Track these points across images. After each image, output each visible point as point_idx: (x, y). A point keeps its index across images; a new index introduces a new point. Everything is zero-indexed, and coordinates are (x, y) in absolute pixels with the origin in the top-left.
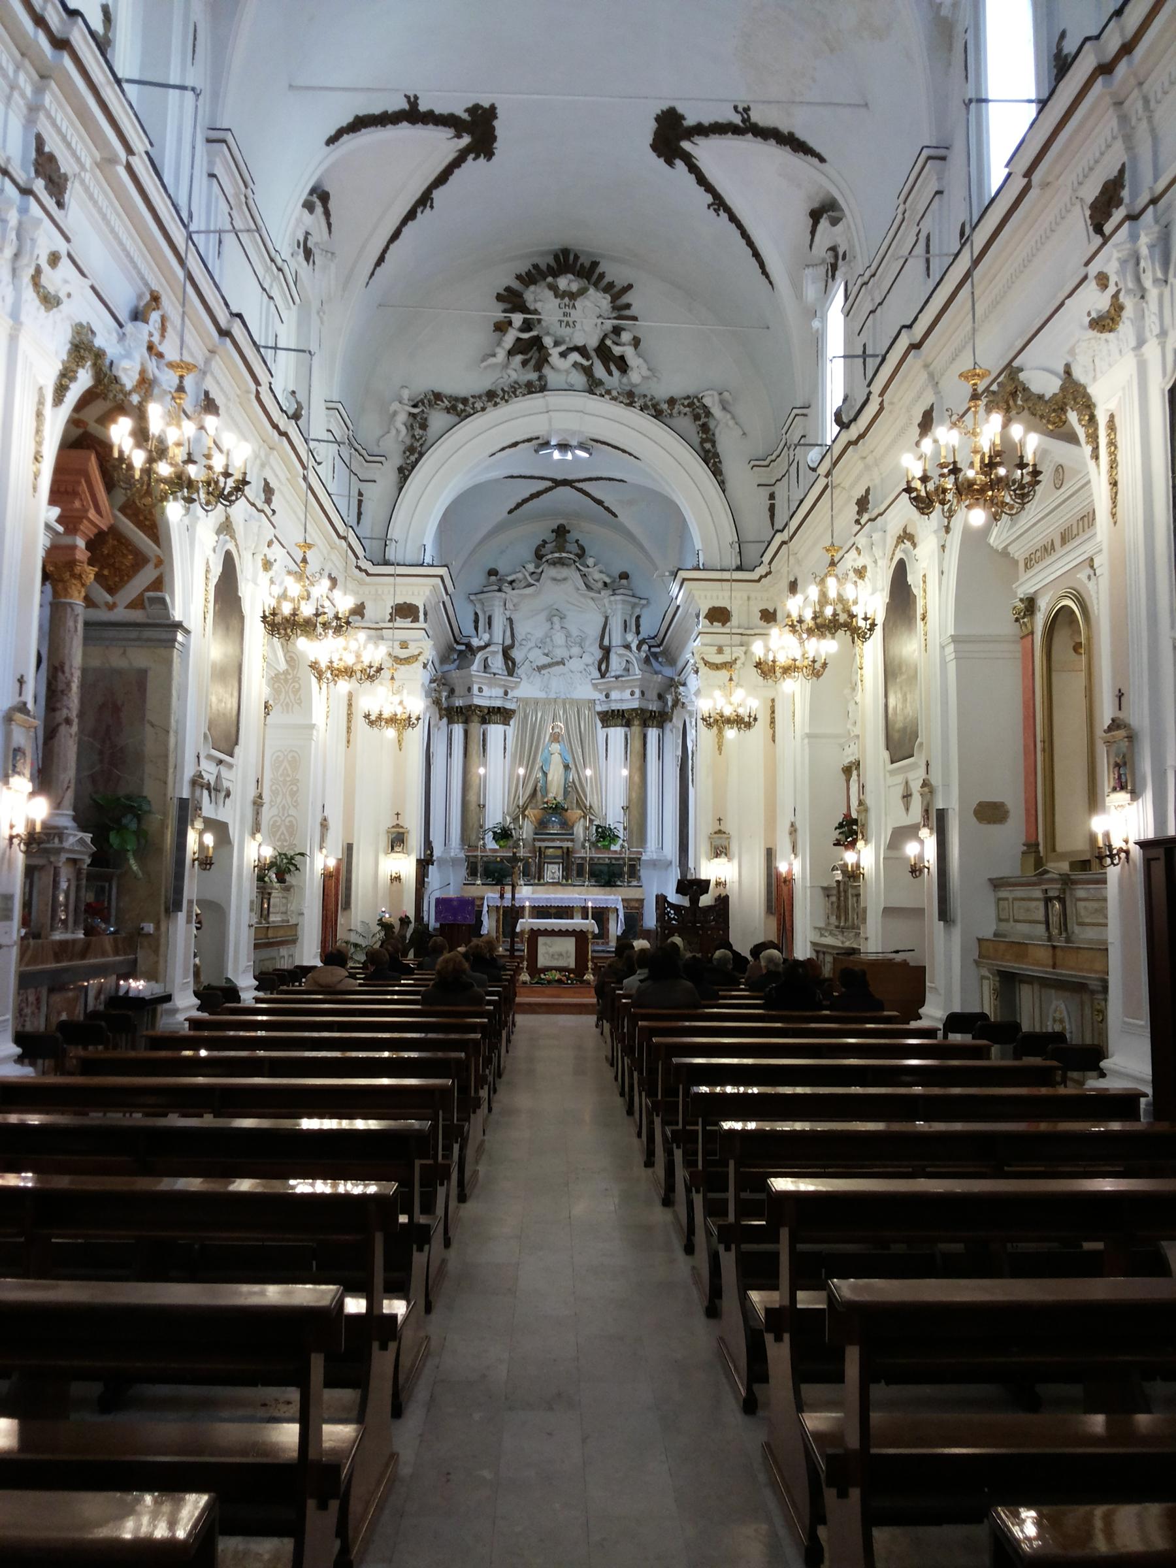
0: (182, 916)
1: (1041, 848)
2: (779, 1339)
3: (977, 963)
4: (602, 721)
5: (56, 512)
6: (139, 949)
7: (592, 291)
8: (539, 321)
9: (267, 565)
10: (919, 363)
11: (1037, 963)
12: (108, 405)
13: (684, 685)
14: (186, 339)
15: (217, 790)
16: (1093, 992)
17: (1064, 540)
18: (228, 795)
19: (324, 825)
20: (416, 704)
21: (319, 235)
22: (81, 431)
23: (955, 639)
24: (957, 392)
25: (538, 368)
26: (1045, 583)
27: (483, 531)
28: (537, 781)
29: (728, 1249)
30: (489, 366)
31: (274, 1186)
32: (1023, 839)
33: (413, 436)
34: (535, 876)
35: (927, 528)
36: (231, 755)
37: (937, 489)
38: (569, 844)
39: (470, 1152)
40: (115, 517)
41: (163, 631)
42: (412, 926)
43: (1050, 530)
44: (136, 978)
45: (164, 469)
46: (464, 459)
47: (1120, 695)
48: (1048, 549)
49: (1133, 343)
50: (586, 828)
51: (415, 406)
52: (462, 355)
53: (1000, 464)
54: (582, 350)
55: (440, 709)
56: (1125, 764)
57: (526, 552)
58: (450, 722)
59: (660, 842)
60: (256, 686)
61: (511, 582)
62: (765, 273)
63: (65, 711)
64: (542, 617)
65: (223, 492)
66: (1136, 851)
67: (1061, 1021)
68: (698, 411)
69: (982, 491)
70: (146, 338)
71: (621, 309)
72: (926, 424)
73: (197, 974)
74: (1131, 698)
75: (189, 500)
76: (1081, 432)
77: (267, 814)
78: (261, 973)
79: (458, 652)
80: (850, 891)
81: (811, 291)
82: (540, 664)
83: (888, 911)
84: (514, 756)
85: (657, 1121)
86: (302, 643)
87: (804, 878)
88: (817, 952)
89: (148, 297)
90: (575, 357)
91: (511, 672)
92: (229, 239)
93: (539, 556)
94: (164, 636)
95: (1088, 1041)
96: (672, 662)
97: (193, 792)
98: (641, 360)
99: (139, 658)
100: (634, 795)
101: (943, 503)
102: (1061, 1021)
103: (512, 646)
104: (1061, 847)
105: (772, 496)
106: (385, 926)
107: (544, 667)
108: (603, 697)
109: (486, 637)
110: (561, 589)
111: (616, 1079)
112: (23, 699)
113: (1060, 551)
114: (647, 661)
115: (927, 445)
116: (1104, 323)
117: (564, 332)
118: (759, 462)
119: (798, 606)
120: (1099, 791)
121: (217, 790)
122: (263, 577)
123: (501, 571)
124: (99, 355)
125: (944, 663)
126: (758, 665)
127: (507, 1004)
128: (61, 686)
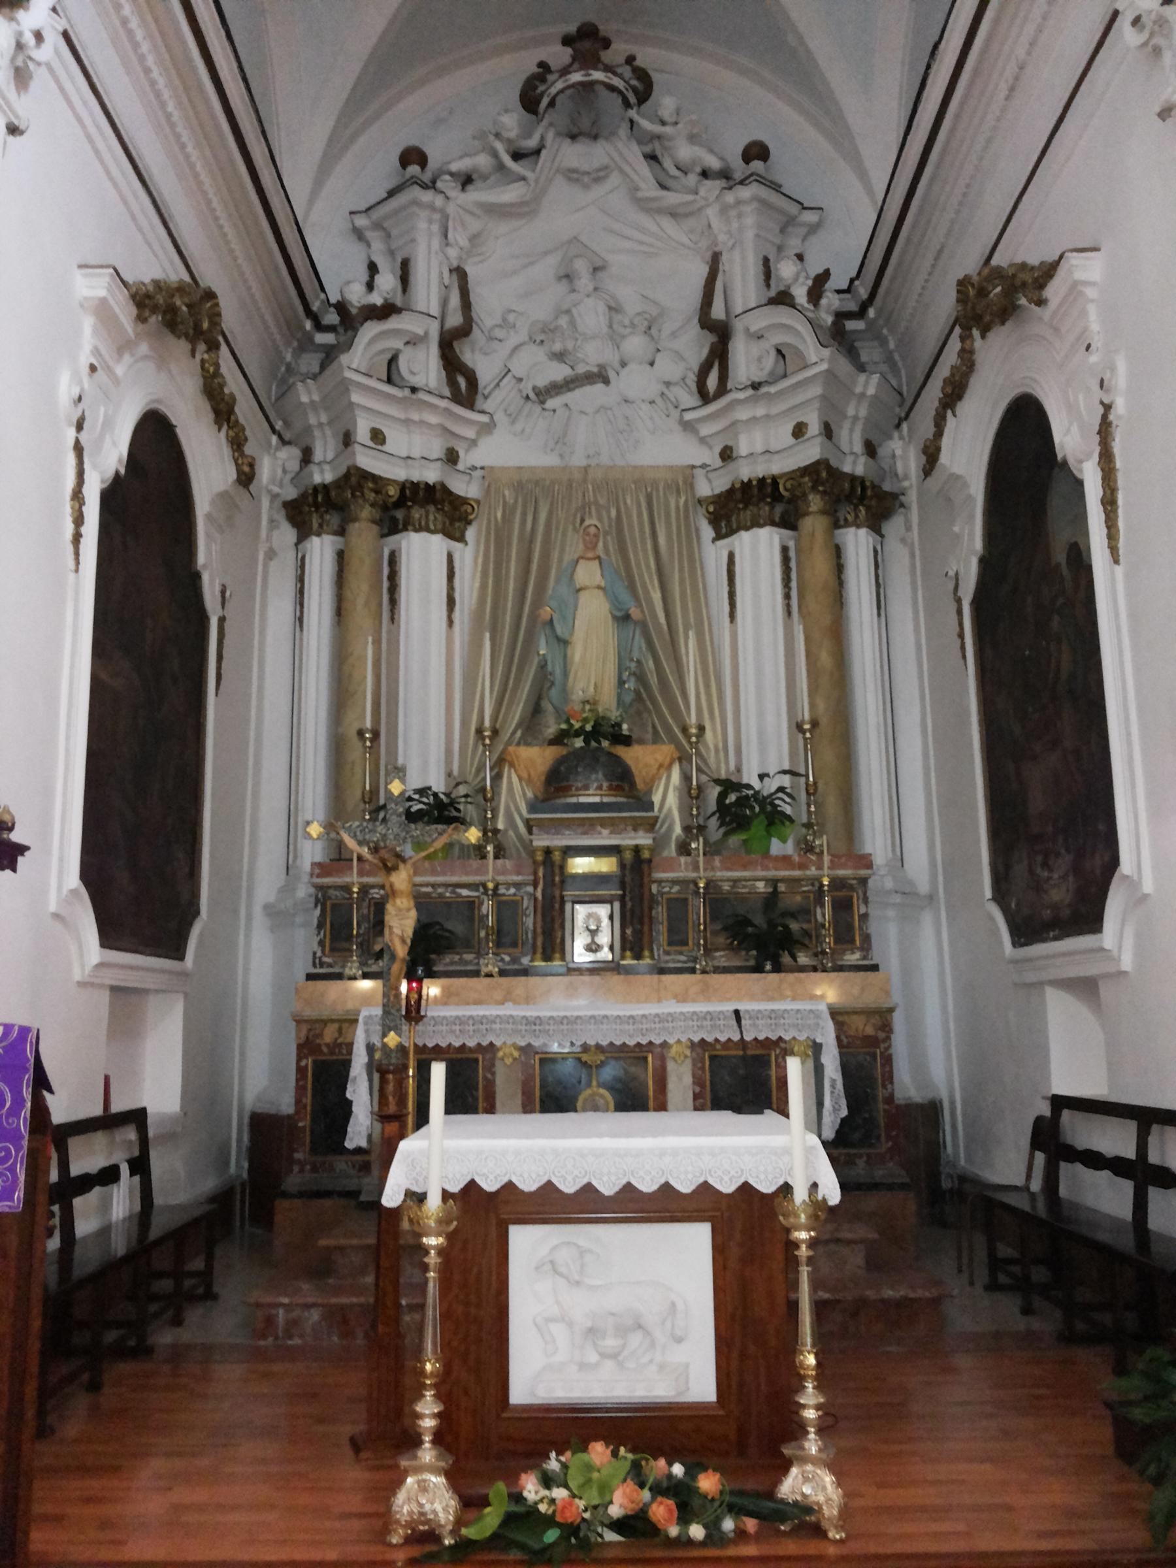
38: (643, 839)
58: (304, 532)
82: (542, 382)
103: (465, 331)
107: (555, 389)
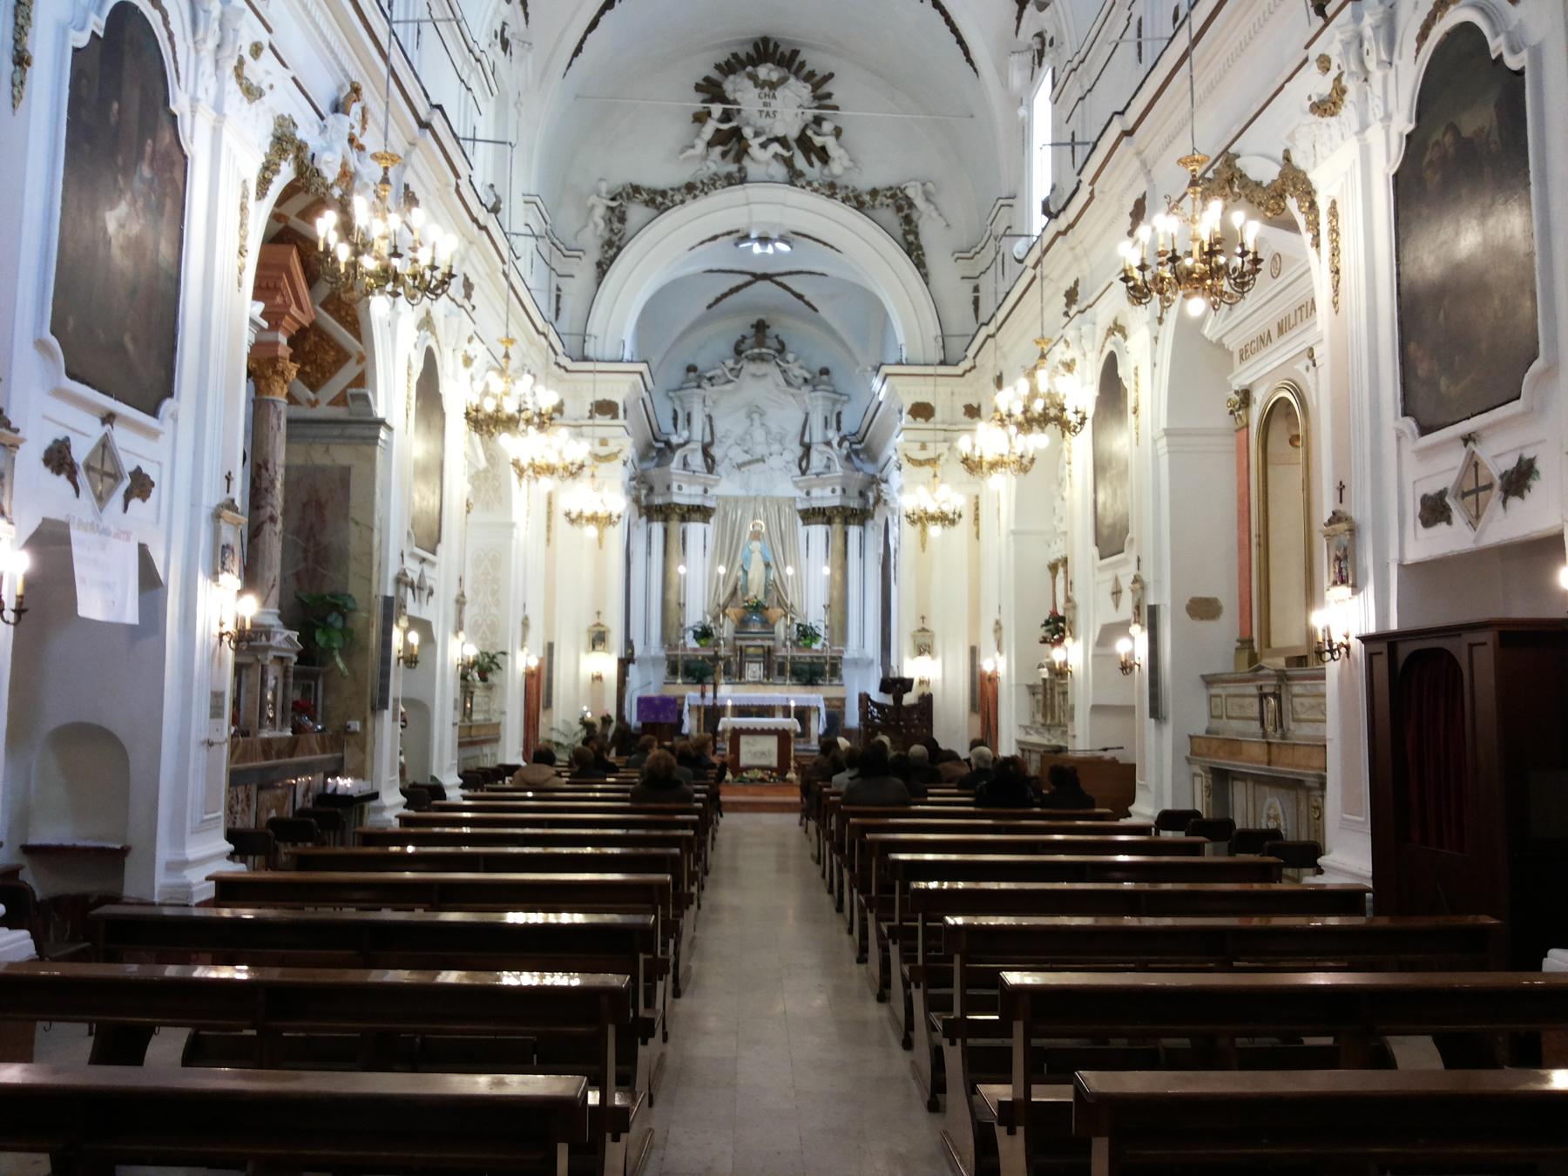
0: (388, 715)
1: (1256, 644)
2: (1011, 1132)
3: (1189, 760)
4: (803, 518)
5: (260, 307)
6: (345, 747)
7: (792, 80)
8: (739, 111)
9: (468, 361)
10: (1131, 150)
11: (1252, 759)
12: (309, 199)
13: (886, 481)
14: (387, 128)
15: (420, 588)
16: (1309, 789)
17: (1281, 331)
18: (431, 593)
19: (525, 624)
20: (616, 501)
21: (516, 26)
22: (281, 226)
23: (1168, 433)
24: (1174, 178)
25: (738, 159)
26: (1262, 376)
27: (681, 328)
28: (737, 579)
29: (953, 1043)
30: (687, 158)
31: (483, 978)
32: (1237, 635)
33: (612, 230)
34: (736, 674)
35: (1139, 319)
36: (434, 553)
37: (1155, 278)
39: (684, 947)
40: (316, 312)
41: (365, 428)
42: (614, 725)
43: (1267, 320)
44: (343, 776)
45: (369, 263)
46: (663, 253)
47: (1341, 488)
48: (1264, 340)
49: (1356, 127)
50: (787, 627)
51: (613, 199)
52: (661, 148)
53: (1220, 252)
54: (782, 141)
55: (640, 508)
56: (1346, 557)
57: (726, 348)
58: (650, 520)
59: (862, 641)
60: (458, 486)
61: (710, 379)
62: (969, 60)
63: (269, 509)
64: (742, 414)
65: (431, 285)
66: (1358, 648)
67: (1276, 818)
68: (901, 203)
69: (1201, 279)
70: (347, 130)
71: (821, 98)
72: (1139, 212)
73: (402, 772)
74: (1352, 492)
75: (395, 294)
76: (1301, 220)
77: (469, 612)
78: (466, 772)
79: (658, 448)
80: (1057, 689)
81: (1017, 78)
83: (1097, 709)
84: (714, 554)
85: (871, 917)
86: (505, 440)
87: (1009, 676)
88: (1023, 750)
89: (348, 89)
90: (776, 148)
91: (710, 470)
92: (428, 28)
93: (738, 351)
94: (367, 433)
95: (1304, 838)
96: (873, 459)
97: (397, 590)
98: (842, 151)
99: (342, 455)
100: (835, 593)
101: (1160, 292)
102: (1276, 818)
103: (711, 443)
104: (1276, 642)
105: (976, 289)
106: (587, 725)
107: (744, 464)
108: (803, 494)
109: (685, 434)
110: (761, 385)
111: (823, 876)
112: (231, 495)
113: (1277, 342)
114: (848, 458)
115: (1143, 231)
116: (1325, 107)
117: (763, 122)
118: (965, 254)
119: (1010, 399)
120: (1317, 585)
121: (420, 588)
122: (465, 374)
123: (700, 367)
124: (301, 147)
125: (1156, 458)
126: (965, 460)
127: (715, 805)
128: (265, 484)
